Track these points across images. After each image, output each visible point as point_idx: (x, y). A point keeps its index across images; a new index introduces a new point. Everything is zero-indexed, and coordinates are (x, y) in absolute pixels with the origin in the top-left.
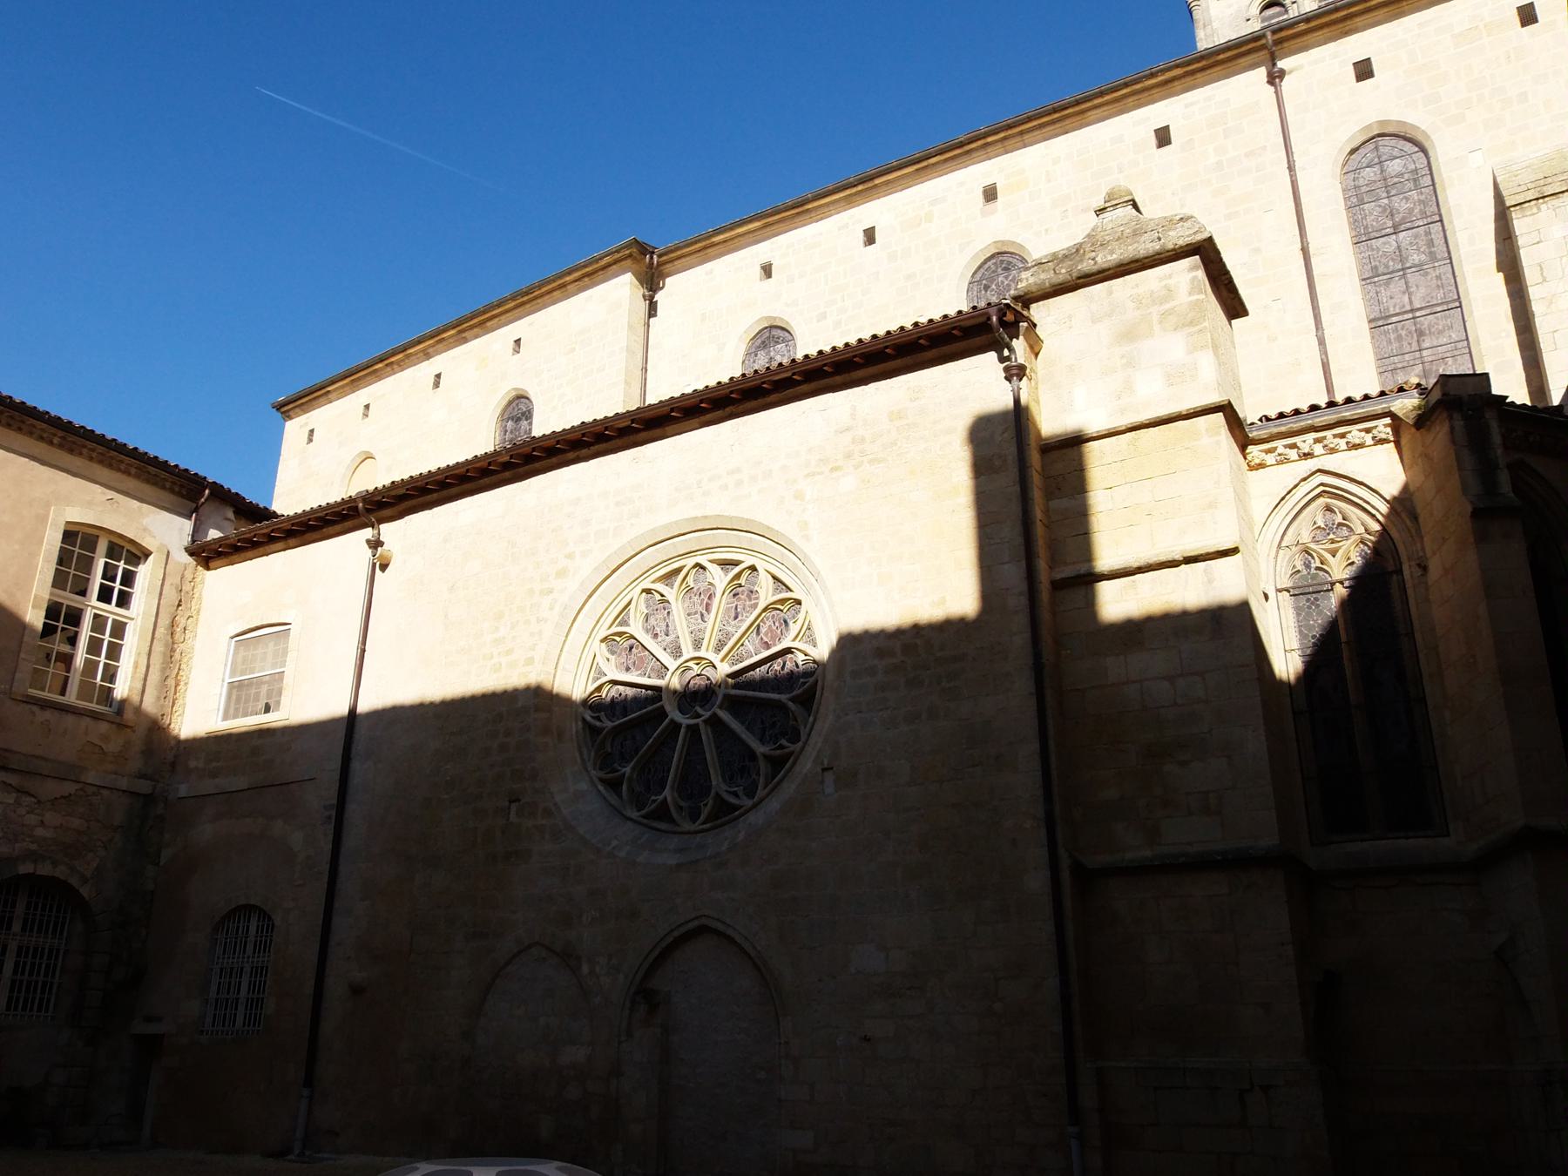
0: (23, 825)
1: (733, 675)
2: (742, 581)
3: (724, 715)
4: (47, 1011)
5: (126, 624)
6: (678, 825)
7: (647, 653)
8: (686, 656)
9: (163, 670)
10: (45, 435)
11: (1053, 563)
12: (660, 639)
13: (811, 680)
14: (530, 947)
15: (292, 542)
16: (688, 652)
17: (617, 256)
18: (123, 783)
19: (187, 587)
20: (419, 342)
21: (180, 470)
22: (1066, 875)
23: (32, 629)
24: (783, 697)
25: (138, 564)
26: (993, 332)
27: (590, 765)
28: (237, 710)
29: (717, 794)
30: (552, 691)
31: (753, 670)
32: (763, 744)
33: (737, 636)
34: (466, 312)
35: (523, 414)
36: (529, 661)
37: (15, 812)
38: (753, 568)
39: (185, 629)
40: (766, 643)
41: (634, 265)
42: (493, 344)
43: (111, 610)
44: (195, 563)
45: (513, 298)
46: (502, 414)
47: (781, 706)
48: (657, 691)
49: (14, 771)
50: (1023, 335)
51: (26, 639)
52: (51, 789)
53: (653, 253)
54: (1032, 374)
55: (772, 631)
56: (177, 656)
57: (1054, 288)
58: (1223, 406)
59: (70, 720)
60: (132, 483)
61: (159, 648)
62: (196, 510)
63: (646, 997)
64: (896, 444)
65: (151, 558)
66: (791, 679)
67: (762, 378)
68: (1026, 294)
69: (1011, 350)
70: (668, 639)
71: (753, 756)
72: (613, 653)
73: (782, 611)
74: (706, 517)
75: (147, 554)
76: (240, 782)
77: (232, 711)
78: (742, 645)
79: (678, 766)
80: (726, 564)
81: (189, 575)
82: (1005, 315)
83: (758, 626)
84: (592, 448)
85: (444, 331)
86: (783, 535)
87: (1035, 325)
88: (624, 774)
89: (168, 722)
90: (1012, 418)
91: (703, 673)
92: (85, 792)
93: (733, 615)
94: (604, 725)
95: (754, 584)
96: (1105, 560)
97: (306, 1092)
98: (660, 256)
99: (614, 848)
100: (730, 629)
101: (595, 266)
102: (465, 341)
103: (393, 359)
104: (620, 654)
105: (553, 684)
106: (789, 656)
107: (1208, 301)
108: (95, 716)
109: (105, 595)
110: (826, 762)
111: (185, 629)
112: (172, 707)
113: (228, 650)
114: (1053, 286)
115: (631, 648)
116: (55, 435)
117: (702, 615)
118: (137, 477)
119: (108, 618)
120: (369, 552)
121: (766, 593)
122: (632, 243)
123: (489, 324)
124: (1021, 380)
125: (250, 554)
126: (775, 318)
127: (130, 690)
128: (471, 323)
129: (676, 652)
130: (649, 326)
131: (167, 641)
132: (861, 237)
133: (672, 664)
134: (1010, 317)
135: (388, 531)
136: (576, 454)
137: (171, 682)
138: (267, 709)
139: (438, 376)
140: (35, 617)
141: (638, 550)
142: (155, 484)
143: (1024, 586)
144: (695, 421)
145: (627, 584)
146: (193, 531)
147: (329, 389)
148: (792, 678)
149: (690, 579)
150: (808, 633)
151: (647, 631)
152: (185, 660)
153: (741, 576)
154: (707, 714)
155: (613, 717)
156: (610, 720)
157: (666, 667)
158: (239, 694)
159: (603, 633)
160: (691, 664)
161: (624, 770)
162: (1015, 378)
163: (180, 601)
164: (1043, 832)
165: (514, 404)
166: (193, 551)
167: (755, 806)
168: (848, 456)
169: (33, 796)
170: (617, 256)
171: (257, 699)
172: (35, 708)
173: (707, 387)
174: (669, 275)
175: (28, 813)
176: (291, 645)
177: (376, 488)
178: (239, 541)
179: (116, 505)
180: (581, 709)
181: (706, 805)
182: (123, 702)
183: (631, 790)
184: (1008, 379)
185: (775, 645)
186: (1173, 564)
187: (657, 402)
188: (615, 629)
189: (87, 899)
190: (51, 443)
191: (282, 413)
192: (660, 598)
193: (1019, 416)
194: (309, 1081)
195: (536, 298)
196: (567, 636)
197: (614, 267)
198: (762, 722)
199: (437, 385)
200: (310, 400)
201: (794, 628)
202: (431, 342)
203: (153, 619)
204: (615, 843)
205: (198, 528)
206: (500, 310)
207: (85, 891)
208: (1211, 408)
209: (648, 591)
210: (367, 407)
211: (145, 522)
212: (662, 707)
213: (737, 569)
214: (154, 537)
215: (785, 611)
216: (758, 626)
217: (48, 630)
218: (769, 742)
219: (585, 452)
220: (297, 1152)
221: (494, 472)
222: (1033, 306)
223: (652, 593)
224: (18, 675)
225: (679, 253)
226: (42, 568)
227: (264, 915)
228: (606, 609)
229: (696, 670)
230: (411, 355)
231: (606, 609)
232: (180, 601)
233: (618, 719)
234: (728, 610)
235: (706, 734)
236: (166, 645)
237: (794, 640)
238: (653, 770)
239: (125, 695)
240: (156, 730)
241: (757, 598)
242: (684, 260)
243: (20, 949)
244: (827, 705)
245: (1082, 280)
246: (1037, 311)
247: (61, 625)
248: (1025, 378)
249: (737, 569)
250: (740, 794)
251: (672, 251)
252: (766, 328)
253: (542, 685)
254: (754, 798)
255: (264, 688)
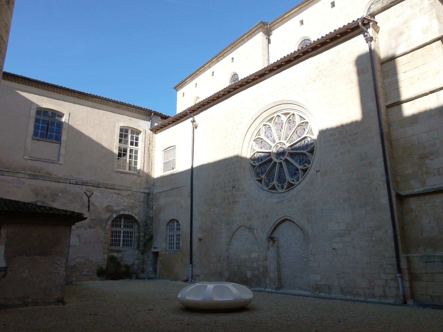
0: (120, 202)
1: (291, 146)
2: (291, 118)
3: (289, 159)
4: (132, 246)
5: (138, 150)
6: (278, 191)
7: (266, 143)
8: (277, 142)
9: (148, 161)
10: (112, 105)
11: (386, 100)
12: (269, 138)
13: (313, 146)
14: (241, 227)
15: (174, 124)
16: (277, 141)
17: (257, 28)
18: (142, 191)
19: (151, 139)
20: (207, 64)
21: (145, 109)
22: (394, 198)
23: (116, 154)
24: (305, 152)
25: (139, 135)
26: (360, 28)
27: (253, 177)
28: (166, 169)
29: (288, 181)
30: (241, 156)
31: (296, 144)
32: (300, 166)
33: (291, 135)
34: (218, 53)
35: (236, 79)
36: (234, 149)
37: (118, 199)
38: (294, 114)
39: (152, 150)
40: (299, 136)
41: (262, 29)
42: (226, 61)
43: (134, 147)
44: (152, 133)
45: (230, 46)
46: (231, 80)
47: (304, 154)
48: (270, 153)
49: (116, 189)
50: (372, 27)
51: (114, 157)
52: (125, 193)
53: (267, 24)
54: (376, 39)
55: (300, 132)
56: (151, 157)
57: (383, 9)
58: (440, 38)
59: (127, 175)
60: (134, 114)
61: (146, 155)
62: (151, 119)
63: (271, 239)
64: (332, 70)
65: (141, 133)
66: (307, 145)
67: (290, 56)
68: (373, 13)
69: (367, 32)
70: (272, 138)
71: (297, 170)
72: (257, 144)
73: (303, 126)
74: (278, 101)
75: (140, 132)
76: (168, 188)
77: (165, 170)
78: (292, 137)
79: (277, 175)
80: (286, 114)
81: (151, 136)
82: (364, 21)
83: (297, 131)
84: (245, 86)
85: (213, 59)
86: (300, 103)
87: (376, 23)
88: (262, 178)
89: (151, 174)
90: (369, 55)
91: (282, 147)
92: (133, 193)
93: (289, 129)
94: (256, 164)
95: (294, 119)
96: (405, 94)
97: (191, 265)
98: (269, 25)
99: (261, 198)
100: (289, 133)
101: (251, 32)
102: (219, 61)
103: (201, 70)
104: (259, 144)
105: (241, 155)
106: (306, 139)
107: (435, 2)
108: (133, 174)
109: (132, 144)
110: (317, 169)
111: (152, 150)
112: (151, 170)
113: (162, 154)
114: (382, 8)
115: (262, 142)
116: (114, 105)
117: (280, 130)
118: (135, 112)
119: (133, 149)
120: (192, 124)
121: (298, 121)
122: (261, 23)
123: (225, 55)
124: (371, 42)
125: (164, 128)
126: (305, 37)
127: (140, 167)
128: (220, 56)
129: (274, 142)
130: (269, 47)
131: (148, 154)
132: (330, 5)
133: (273, 145)
134: (366, 22)
135: (196, 117)
136: (241, 88)
137: (150, 164)
138: (173, 169)
139: (213, 72)
140: (116, 151)
141: (260, 113)
142: (140, 114)
143: (376, 109)
144: (273, 73)
145: (259, 124)
146: (151, 125)
147: (186, 81)
148: (307, 145)
149: (276, 121)
150: (311, 132)
151: (266, 136)
152: (153, 158)
153: (290, 117)
154: (284, 159)
155: (259, 162)
156: (258, 163)
157: (272, 146)
158: (167, 165)
159: (254, 138)
160: (278, 145)
161: (262, 177)
162: (369, 42)
163: (150, 143)
164: (386, 185)
165: (234, 77)
166: (151, 130)
167: (299, 184)
168: (318, 76)
169: (121, 195)
170: (257, 28)
171: (170, 166)
172: (119, 174)
173: (274, 62)
174: (273, 30)
175: (121, 199)
176: (176, 151)
177: (191, 106)
178: (161, 125)
179: (131, 120)
180: (250, 161)
181: (285, 185)
182: (139, 170)
183: (265, 182)
184: (367, 42)
185: (302, 136)
186: (426, 94)
187: (261, 69)
188: (257, 137)
189: (137, 219)
190: (114, 107)
191: (176, 90)
192: (268, 126)
193: (372, 54)
194: (191, 263)
195: (236, 45)
196: (244, 141)
197: (257, 31)
198: (300, 159)
199: (213, 75)
200: (182, 85)
201: (307, 131)
202: (210, 63)
203: (144, 148)
204: (261, 197)
205: (152, 124)
206: (227, 50)
207: (136, 218)
208: (437, 39)
209: (265, 125)
210: (196, 84)
211: (139, 124)
212: (271, 158)
213: (289, 115)
214: (142, 127)
215: (304, 126)
216: (297, 131)
217: (120, 155)
218: (302, 165)
219: (243, 87)
220: (190, 280)
221: (220, 97)
222: (376, 17)
223: (266, 126)
224: (114, 166)
225: (275, 23)
226: (116, 139)
227: (177, 222)
228: (254, 132)
229: (280, 146)
230: (205, 68)
231: (254, 132)
232: (150, 143)
233: (260, 162)
234: (287, 128)
235: (284, 164)
236: (148, 155)
237: (307, 134)
238: (270, 176)
239: (140, 169)
240: (148, 176)
241: (296, 123)
242: (277, 25)
243: (124, 232)
244: (317, 152)
245: (392, 4)
246: (377, 18)
247: (122, 152)
248: (373, 41)
249: (289, 115)
250: (295, 180)
251: (273, 23)
252: (303, 40)
253: (238, 155)
254: (298, 181)
255: (172, 163)
